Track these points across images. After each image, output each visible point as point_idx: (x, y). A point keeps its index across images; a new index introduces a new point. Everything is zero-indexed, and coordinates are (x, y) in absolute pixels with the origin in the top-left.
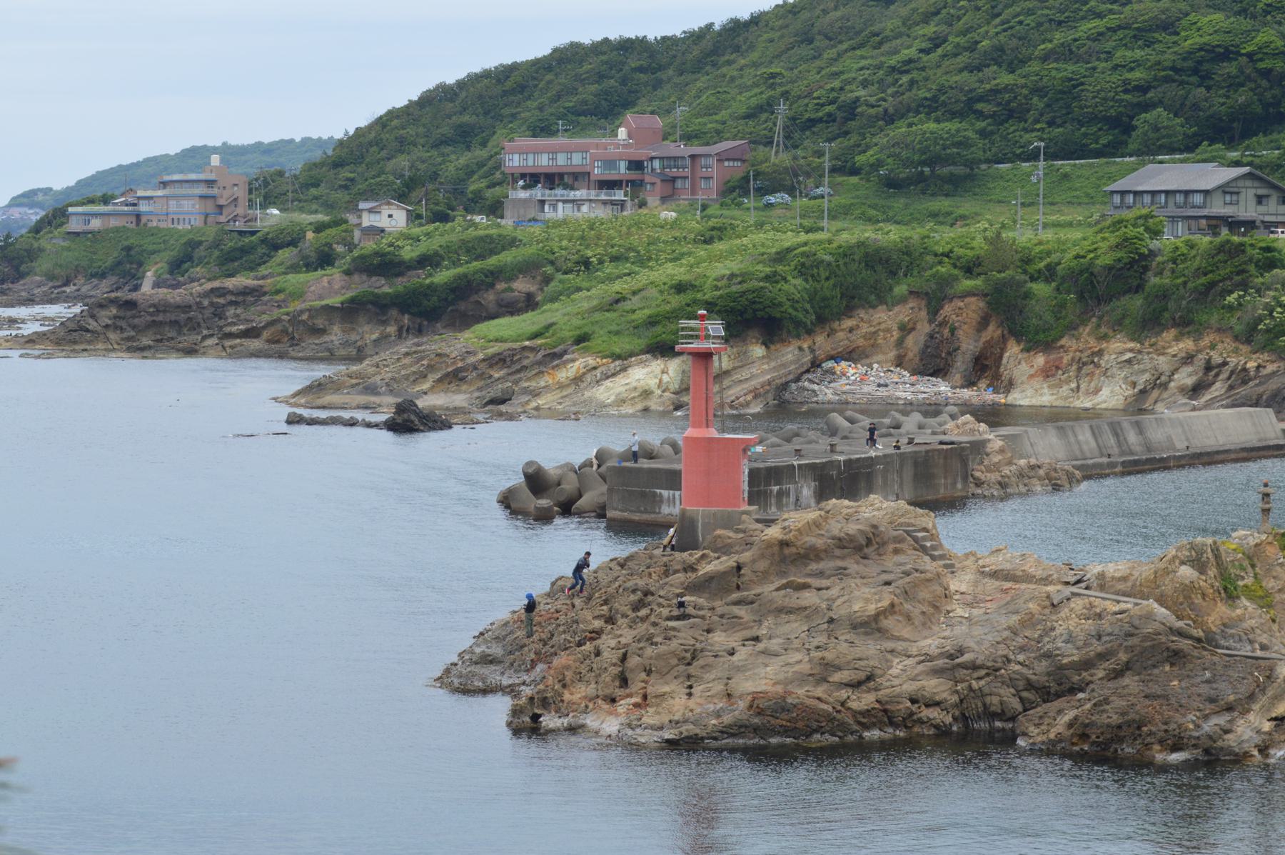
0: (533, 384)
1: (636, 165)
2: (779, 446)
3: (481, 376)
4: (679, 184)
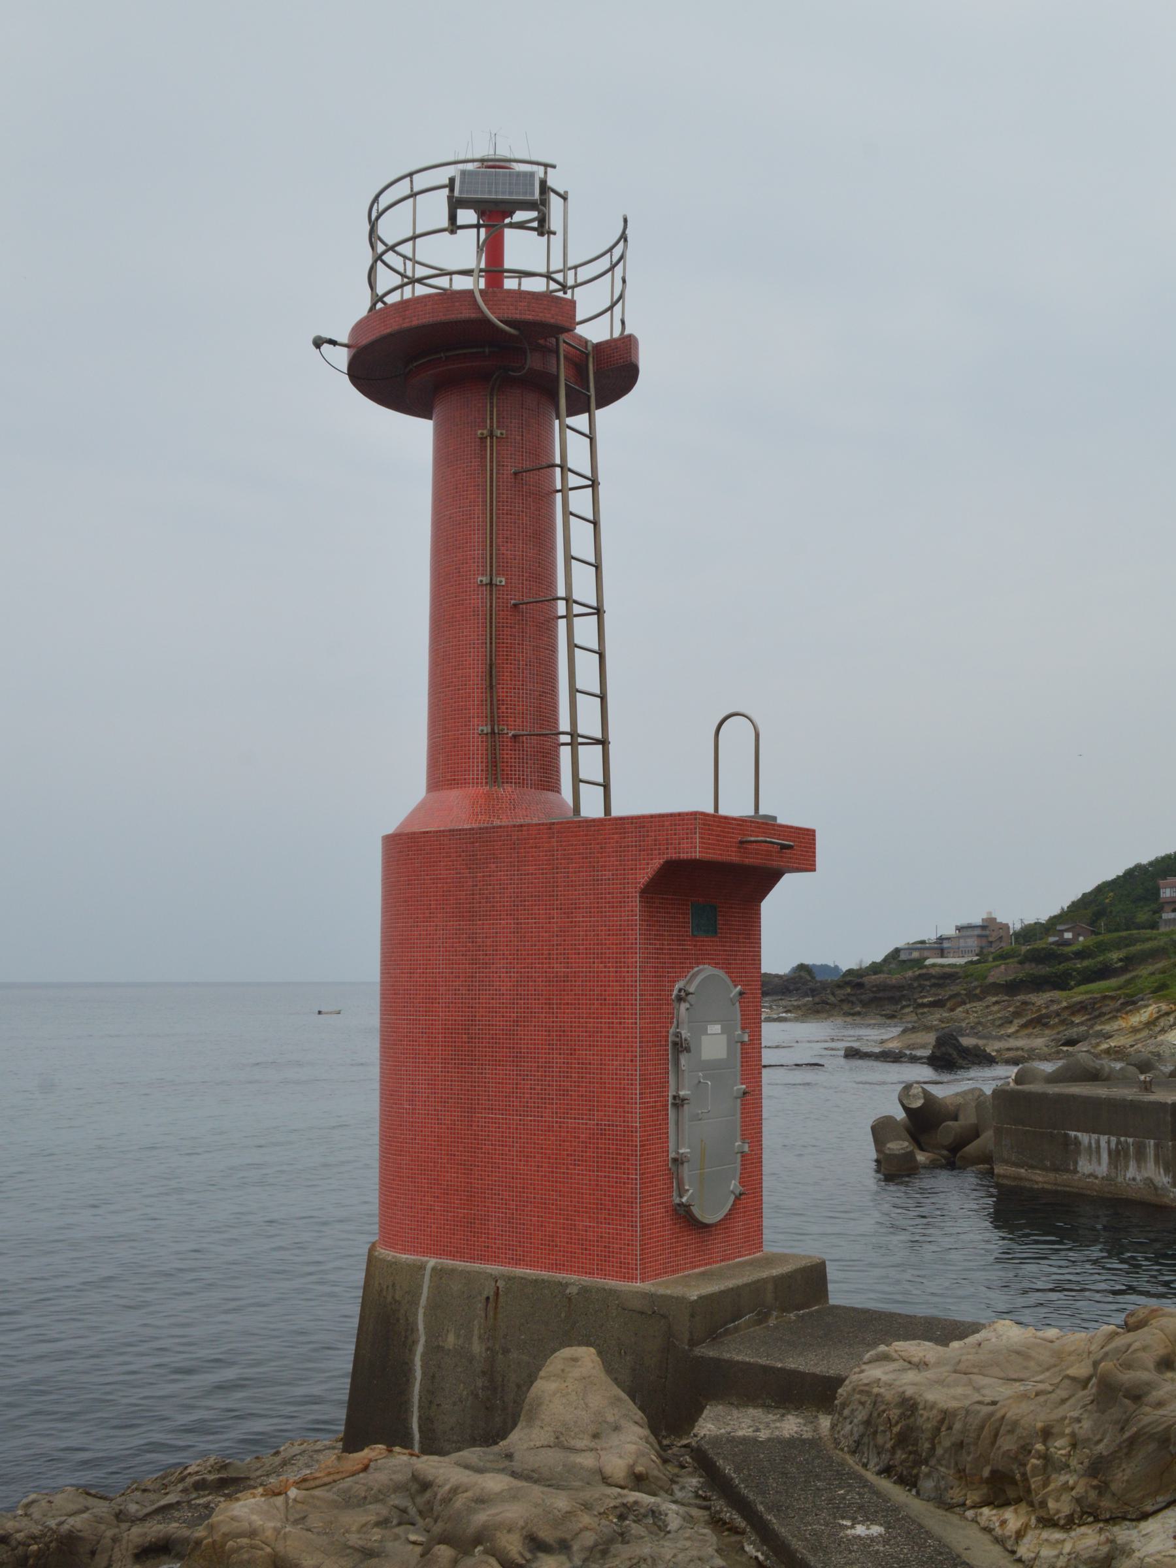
0: (1107, 1028)
3: (1063, 1022)
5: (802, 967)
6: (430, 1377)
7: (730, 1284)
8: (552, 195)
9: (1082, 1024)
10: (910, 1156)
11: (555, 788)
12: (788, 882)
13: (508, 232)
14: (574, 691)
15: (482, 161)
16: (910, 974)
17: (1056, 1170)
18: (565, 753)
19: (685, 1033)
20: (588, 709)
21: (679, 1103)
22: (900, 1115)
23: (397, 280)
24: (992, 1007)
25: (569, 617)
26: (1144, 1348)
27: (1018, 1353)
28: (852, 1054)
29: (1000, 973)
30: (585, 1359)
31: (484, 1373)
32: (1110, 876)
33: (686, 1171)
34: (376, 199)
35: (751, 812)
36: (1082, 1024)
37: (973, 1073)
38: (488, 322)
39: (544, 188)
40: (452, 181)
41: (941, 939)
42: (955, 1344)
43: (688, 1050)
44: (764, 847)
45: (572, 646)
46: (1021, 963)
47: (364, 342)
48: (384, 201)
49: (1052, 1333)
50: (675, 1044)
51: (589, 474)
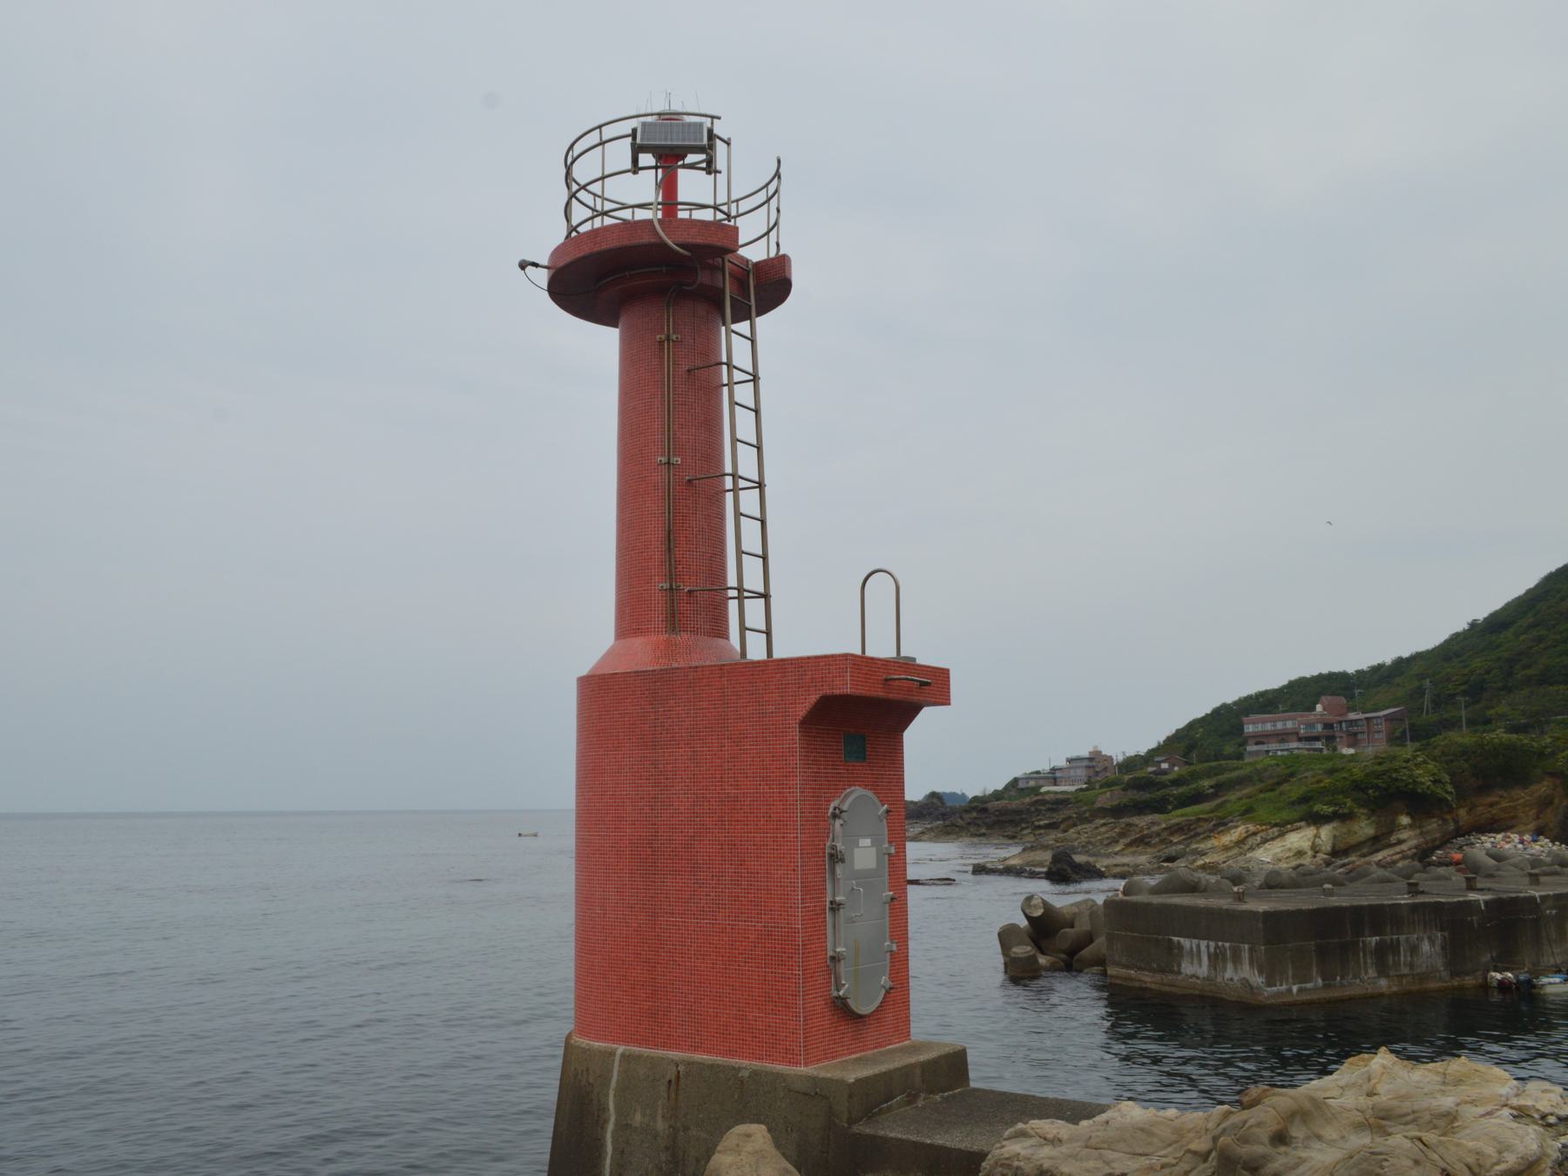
0: (1202, 846)
1: (1329, 726)
2: (1389, 881)
3: (1163, 841)
4: (1360, 737)
5: (933, 795)
6: (620, 1152)
7: (883, 1068)
8: (718, 142)
9: (1179, 843)
10: (1033, 959)
11: (723, 633)
12: (926, 713)
13: (680, 171)
14: (740, 552)
15: (659, 114)
16: (1027, 800)
17: (1162, 971)
18: (733, 606)
19: (840, 846)
20: (752, 567)
21: (836, 907)
22: (1023, 923)
23: (589, 213)
24: (1101, 829)
25: (736, 490)
26: (1259, 1125)
27: (1142, 1130)
28: (979, 870)
29: (1106, 799)
30: (759, 1133)
31: (667, 1148)
32: (1200, 715)
33: (842, 968)
34: (571, 147)
35: (894, 655)
36: (1179, 843)
37: (1085, 885)
38: (665, 245)
39: (711, 135)
40: (634, 131)
41: (1054, 770)
42: (1084, 1123)
43: (842, 861)
44: (905, 684)
45: (738, 514)
46: (1124, 790)
47: (561, 264)
48: (578, 149)
49: (1172, 1112)
50: (831, 855)
51: (750, 370)
